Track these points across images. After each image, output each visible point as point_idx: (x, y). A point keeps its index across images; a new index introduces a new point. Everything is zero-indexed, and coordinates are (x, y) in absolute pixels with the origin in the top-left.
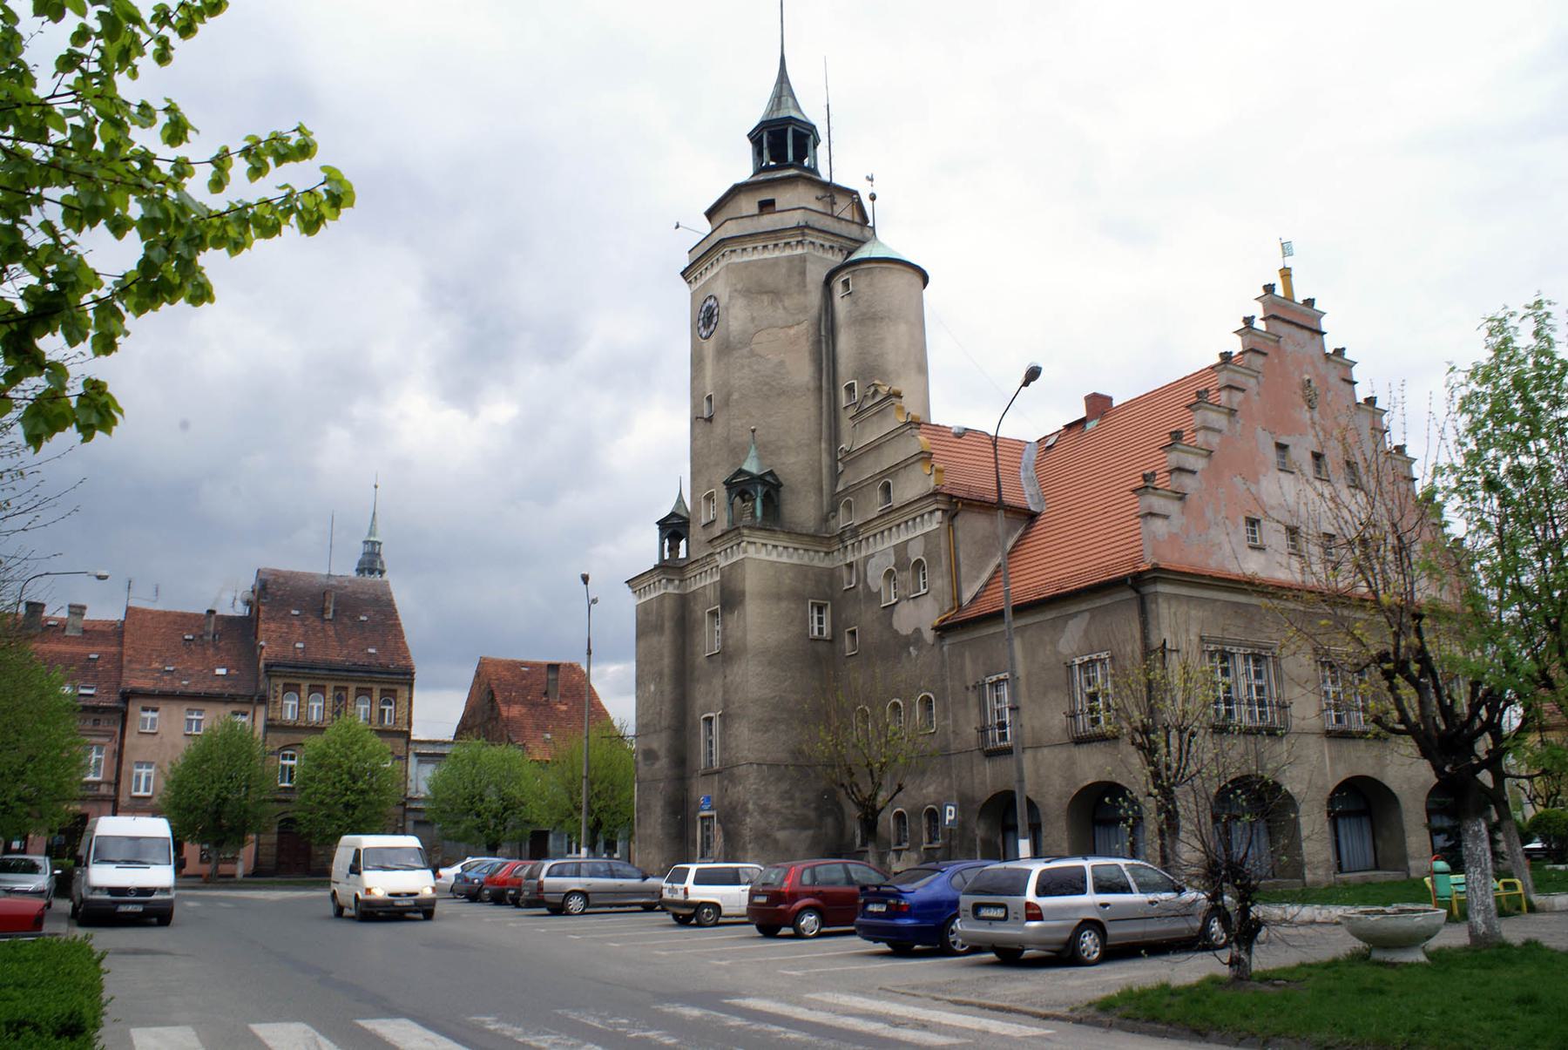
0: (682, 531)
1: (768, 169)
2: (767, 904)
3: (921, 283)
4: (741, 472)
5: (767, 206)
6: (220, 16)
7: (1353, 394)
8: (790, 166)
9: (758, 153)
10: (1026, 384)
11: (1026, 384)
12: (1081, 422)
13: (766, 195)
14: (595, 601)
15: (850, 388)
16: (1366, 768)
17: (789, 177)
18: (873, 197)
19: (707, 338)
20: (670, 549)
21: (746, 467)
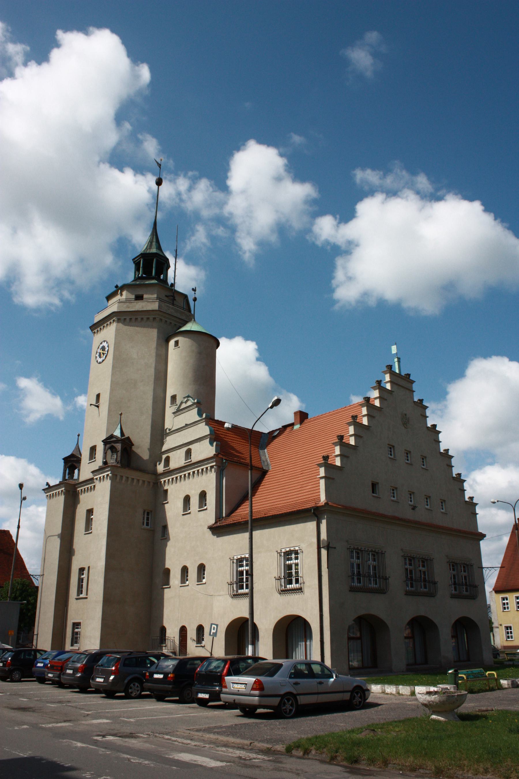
0: (76, 465)
1: (141, 278)
2: (103, 682)
3: (216, 346)
4: (112, 436)
5: (139, 298)
6: (181, 625)
7: (412, 398)
8: (153, 278)
9: (137, 269)
10: (272, 407)
11: (272, 407)
12: (292, 425)
13: (140, 293)
14: (25, 499)
15: (174, 398)
16: (422, 612)
17: (408, 575)
18: (195, 300)
19: (100, 363)
20: (69, 474)
21: (115, 434)
